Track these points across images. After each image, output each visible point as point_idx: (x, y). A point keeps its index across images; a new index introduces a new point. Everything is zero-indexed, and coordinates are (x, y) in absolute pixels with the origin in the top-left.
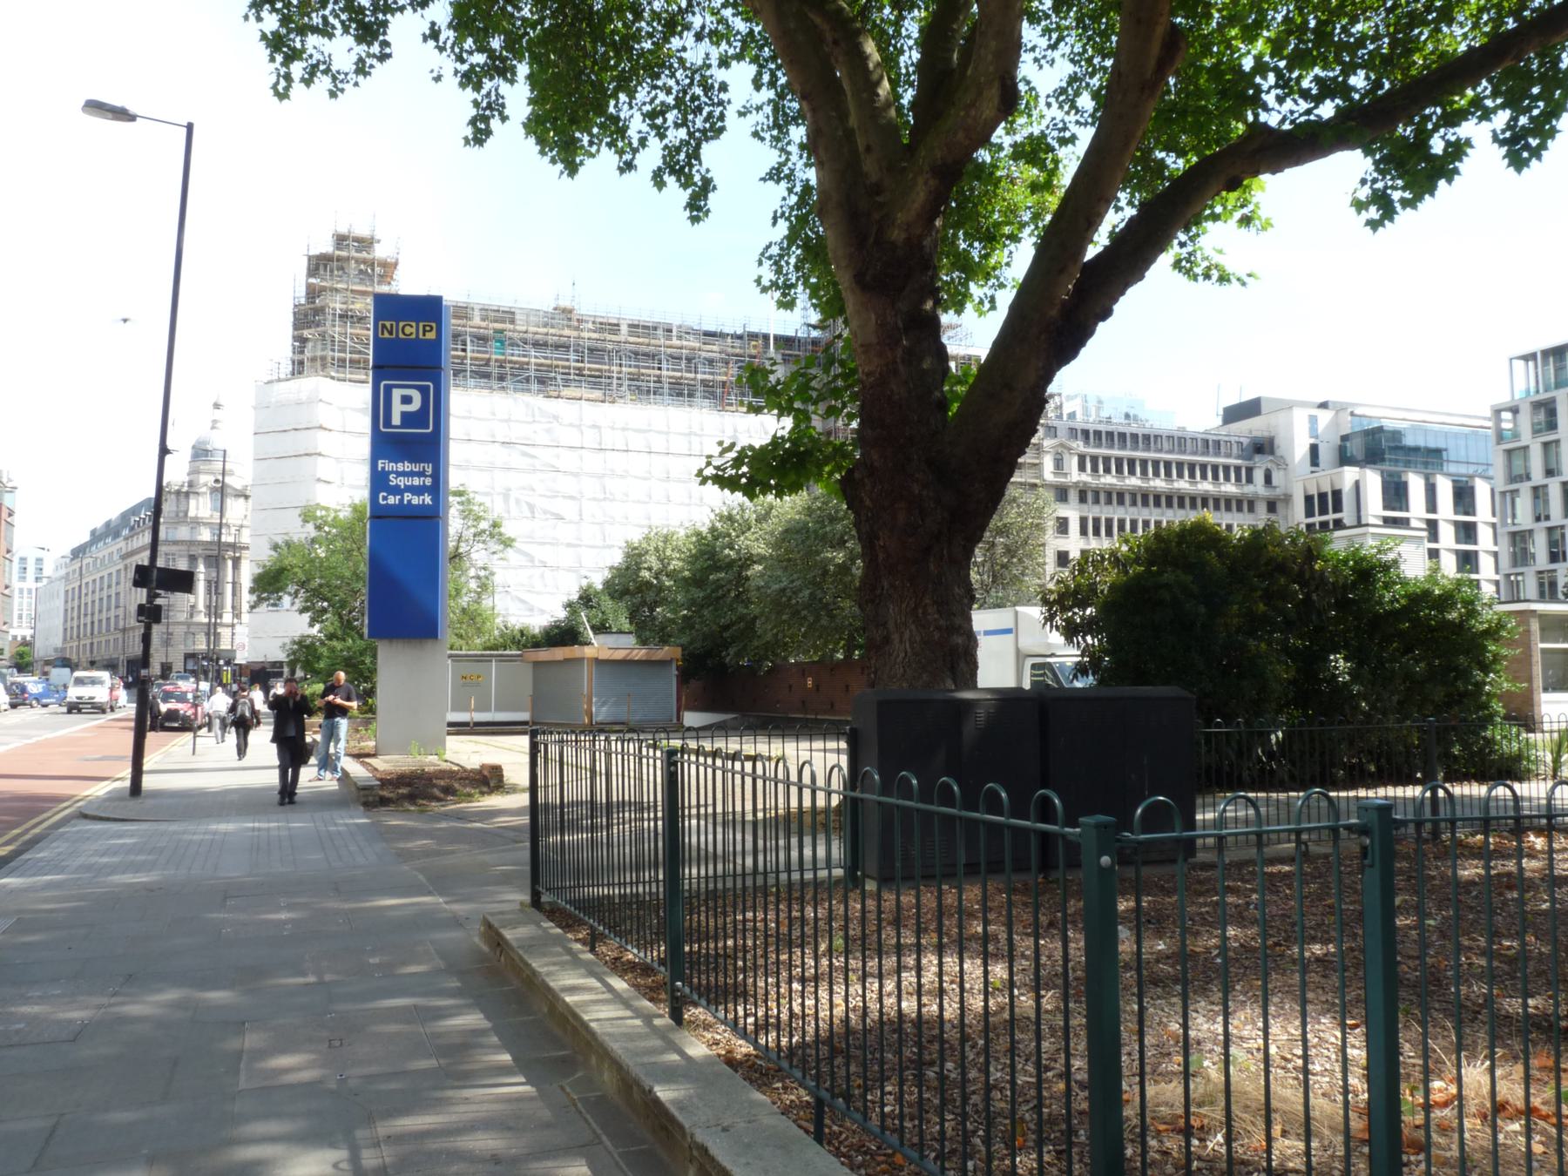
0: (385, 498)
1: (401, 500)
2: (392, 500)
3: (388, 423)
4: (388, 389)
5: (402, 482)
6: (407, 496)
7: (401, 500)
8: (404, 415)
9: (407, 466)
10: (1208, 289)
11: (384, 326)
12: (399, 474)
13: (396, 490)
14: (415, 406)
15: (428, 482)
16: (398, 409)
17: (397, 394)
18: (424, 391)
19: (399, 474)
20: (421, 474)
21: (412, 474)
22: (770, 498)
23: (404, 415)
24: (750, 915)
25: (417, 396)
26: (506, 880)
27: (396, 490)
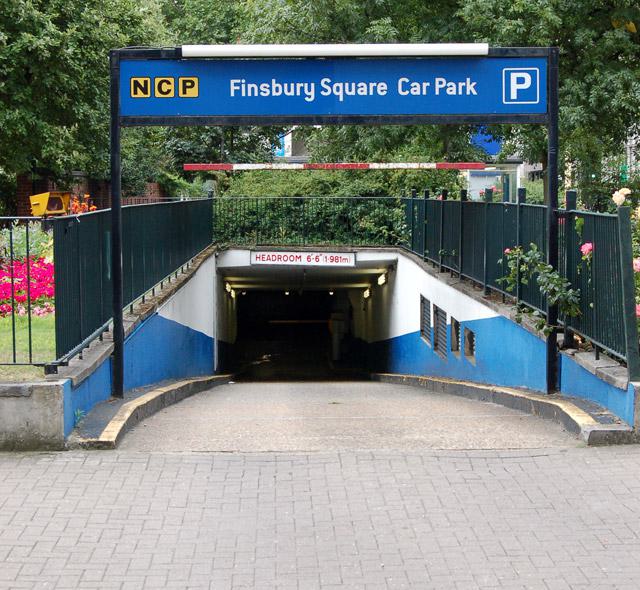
8: (518, 90)
14: (527, 84)
17: (514, 77)
18: (533, 74)
23: (518, 90)
25: (528, 78)
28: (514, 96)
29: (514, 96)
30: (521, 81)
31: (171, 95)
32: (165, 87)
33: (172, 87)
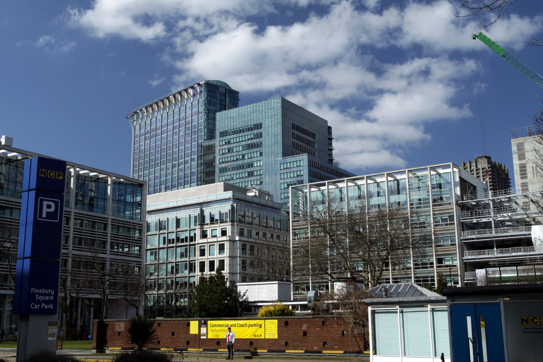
0: (33, 306)
1: (40, 307)
2: (36, 307)
3: (41, 216)
4: (42, 201)
5: (41, 298)
6: (43, 305)
7: (40, 307)
8: (47, 213)
9: (44, 291)
10: (488, 156)
11: (42, 171)
12: (40, 294)
13: (38, 302)
14: (52, 210)
15: (52, 298)
16: (45, 210)
17: (45, 203)
18: (56, 203)
19: (40, 294)
20: (49, 295)
21: (45, 295)
22: (221, 56)
23: (47, 213)
24: (249, 118)
25: (53, 205)
26: (94, 349)
27: (38, 302)
28: (44, 215)
29: (44, 215)
30: (49, 207)
31: (54, 177)
32: (52, 174)
33: (54, 175)
